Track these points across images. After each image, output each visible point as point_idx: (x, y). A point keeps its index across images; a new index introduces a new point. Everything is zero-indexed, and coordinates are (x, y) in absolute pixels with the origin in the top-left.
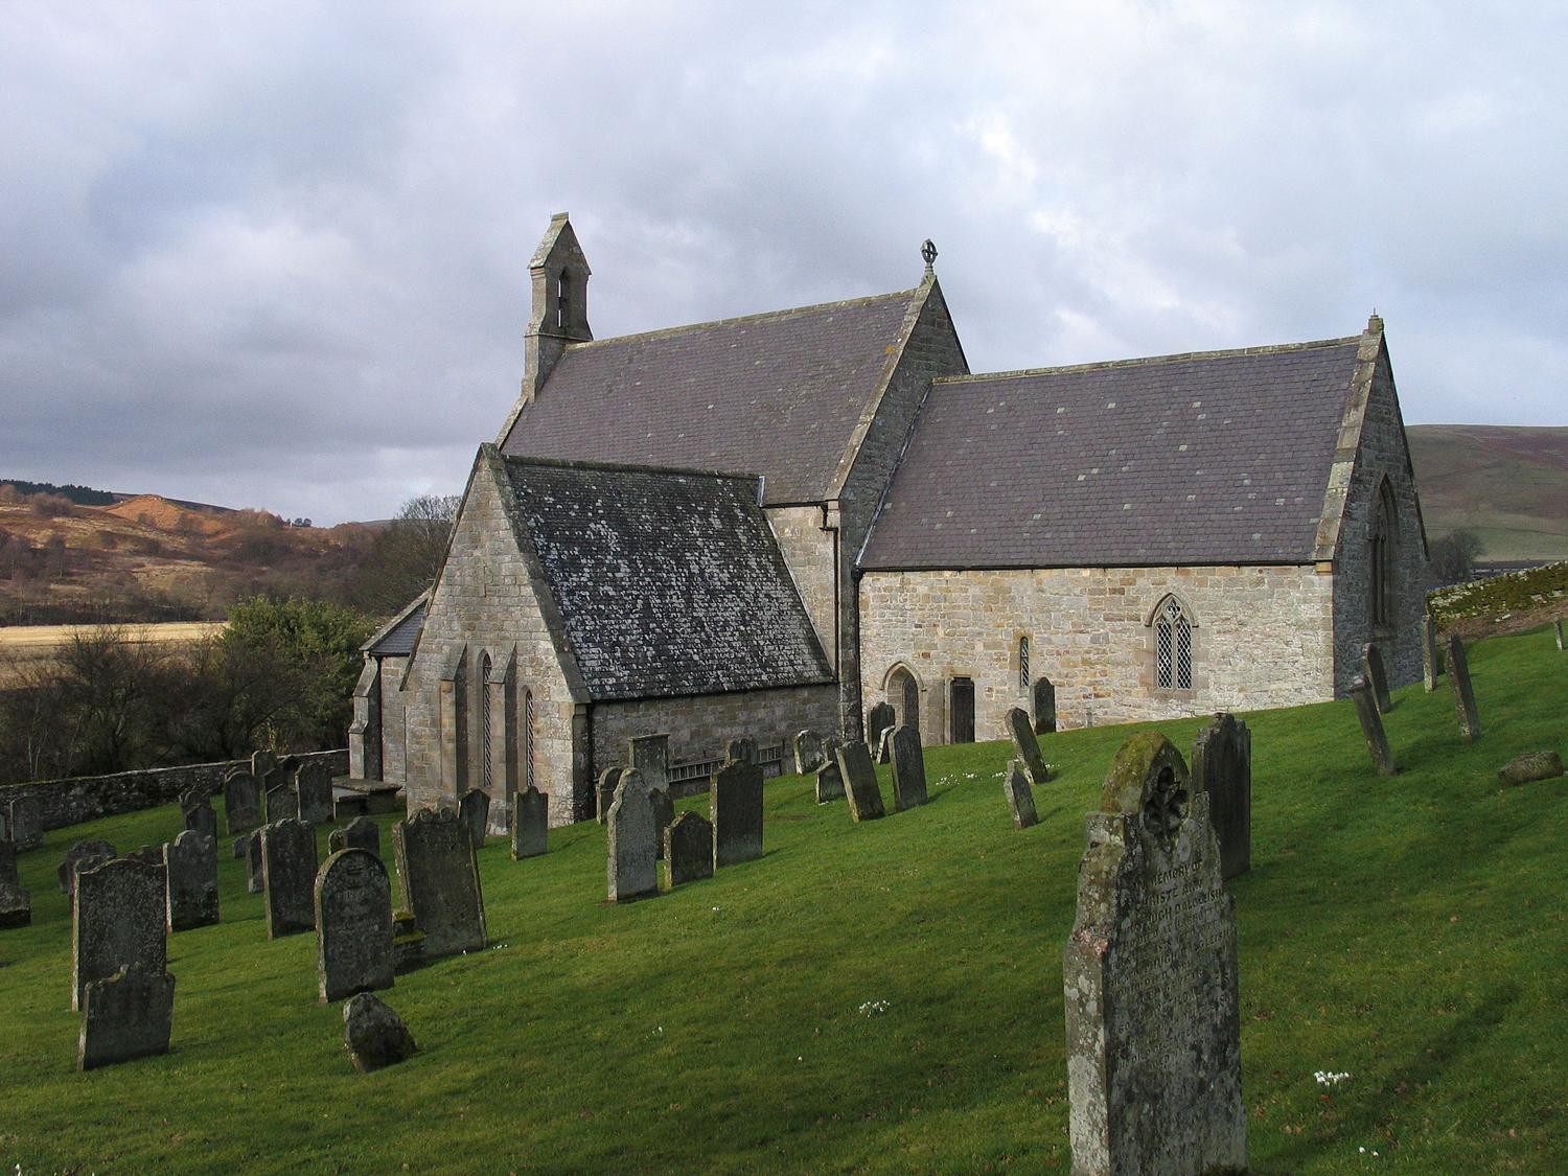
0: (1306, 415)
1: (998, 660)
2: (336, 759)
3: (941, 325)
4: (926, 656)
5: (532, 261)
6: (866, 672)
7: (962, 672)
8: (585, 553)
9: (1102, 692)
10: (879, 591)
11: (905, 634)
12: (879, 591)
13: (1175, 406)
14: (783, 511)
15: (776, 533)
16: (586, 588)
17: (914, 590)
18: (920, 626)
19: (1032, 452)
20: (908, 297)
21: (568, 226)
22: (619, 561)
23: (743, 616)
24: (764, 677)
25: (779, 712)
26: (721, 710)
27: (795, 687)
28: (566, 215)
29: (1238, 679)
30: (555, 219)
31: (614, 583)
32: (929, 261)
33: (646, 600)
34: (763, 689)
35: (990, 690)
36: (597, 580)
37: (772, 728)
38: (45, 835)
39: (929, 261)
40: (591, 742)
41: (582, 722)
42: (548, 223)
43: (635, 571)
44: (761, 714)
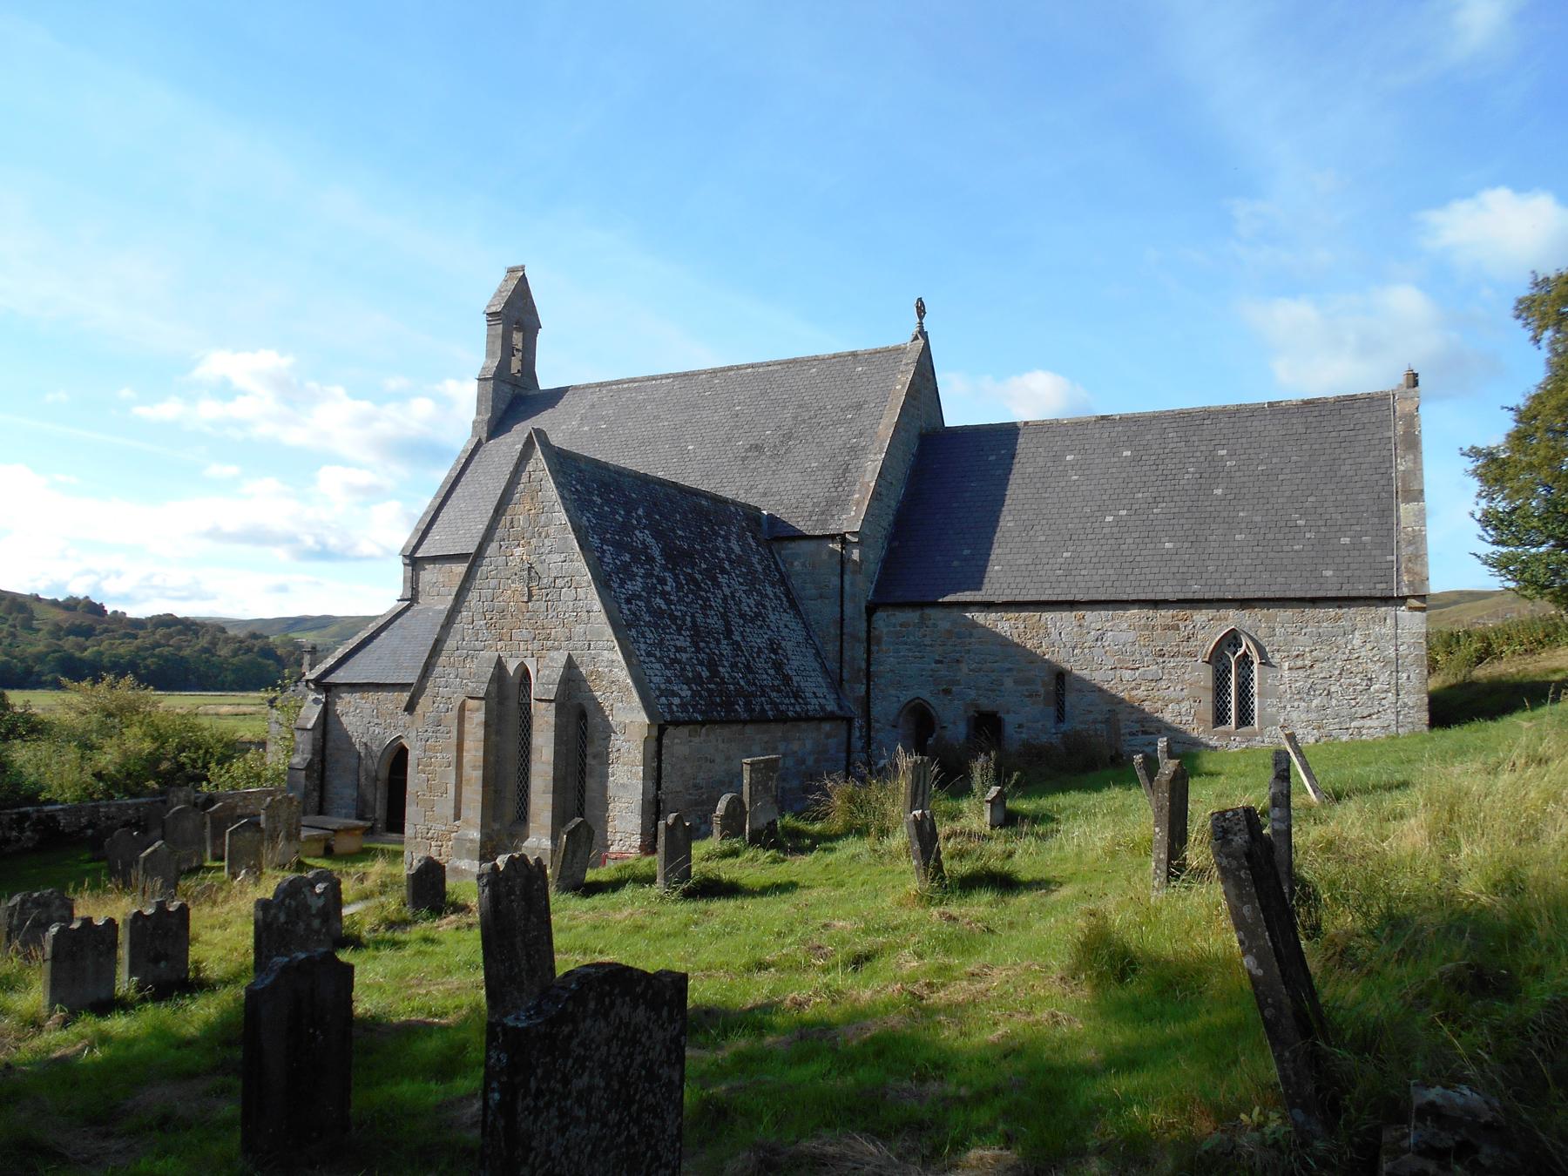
0: (1350, 461)
1: (1030, 696)
2: (256, 798)
3: (928, 380)
4: (947, 692)
5: (488, 307)
6: (877, 709)
7: (986, 704)
8: (635, 560)
9: (1151, 730)
10: (894, 626)
11: (923, 670)
12: (894, 626)
13: (1198, 454)
14: (792, 545)
15: (784, 565)
16: (639, 597)
17: (935, 625)
18: (941, 662)
19: (1047, 495)
20: (898, 351)
21: (523, 279)
22: (666, 574)
23: (771, 644)
24: (798, 709)
25: (809, 745)
26: (766, 740)
27: (821, 720)
28: (523, 268)
29: (1313, 716)
30: (512, 271)
31: (664, 595)
32: (921, 318)
33: (693, 616)
34: (798, 719)
35: (1020, 726)
36: (651, 590)
37: (803, 762)
38: (303, 818)
39: (921, 318)
40: (659, 768)
41: (653, 744)
42: (502, 275)
43: (679, 587)
44: (795, 746)
